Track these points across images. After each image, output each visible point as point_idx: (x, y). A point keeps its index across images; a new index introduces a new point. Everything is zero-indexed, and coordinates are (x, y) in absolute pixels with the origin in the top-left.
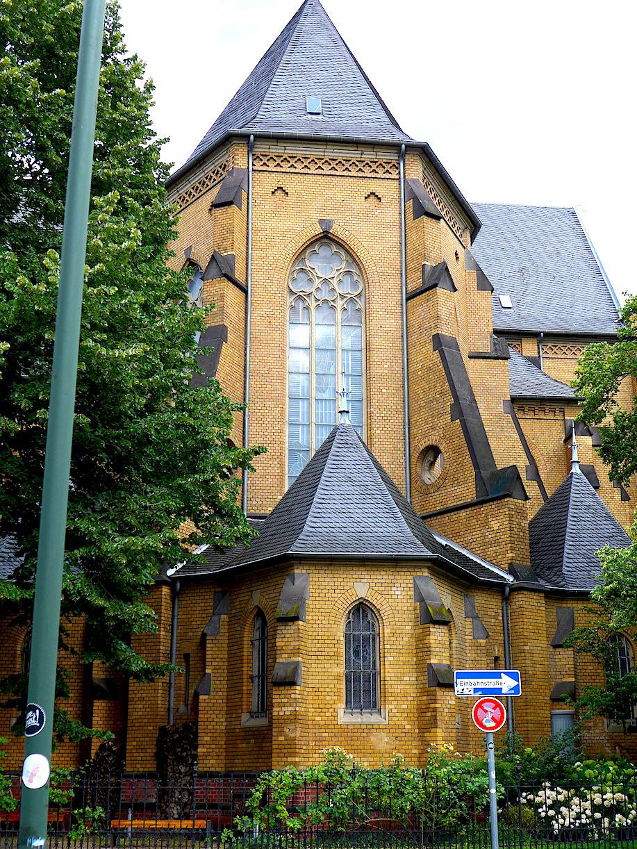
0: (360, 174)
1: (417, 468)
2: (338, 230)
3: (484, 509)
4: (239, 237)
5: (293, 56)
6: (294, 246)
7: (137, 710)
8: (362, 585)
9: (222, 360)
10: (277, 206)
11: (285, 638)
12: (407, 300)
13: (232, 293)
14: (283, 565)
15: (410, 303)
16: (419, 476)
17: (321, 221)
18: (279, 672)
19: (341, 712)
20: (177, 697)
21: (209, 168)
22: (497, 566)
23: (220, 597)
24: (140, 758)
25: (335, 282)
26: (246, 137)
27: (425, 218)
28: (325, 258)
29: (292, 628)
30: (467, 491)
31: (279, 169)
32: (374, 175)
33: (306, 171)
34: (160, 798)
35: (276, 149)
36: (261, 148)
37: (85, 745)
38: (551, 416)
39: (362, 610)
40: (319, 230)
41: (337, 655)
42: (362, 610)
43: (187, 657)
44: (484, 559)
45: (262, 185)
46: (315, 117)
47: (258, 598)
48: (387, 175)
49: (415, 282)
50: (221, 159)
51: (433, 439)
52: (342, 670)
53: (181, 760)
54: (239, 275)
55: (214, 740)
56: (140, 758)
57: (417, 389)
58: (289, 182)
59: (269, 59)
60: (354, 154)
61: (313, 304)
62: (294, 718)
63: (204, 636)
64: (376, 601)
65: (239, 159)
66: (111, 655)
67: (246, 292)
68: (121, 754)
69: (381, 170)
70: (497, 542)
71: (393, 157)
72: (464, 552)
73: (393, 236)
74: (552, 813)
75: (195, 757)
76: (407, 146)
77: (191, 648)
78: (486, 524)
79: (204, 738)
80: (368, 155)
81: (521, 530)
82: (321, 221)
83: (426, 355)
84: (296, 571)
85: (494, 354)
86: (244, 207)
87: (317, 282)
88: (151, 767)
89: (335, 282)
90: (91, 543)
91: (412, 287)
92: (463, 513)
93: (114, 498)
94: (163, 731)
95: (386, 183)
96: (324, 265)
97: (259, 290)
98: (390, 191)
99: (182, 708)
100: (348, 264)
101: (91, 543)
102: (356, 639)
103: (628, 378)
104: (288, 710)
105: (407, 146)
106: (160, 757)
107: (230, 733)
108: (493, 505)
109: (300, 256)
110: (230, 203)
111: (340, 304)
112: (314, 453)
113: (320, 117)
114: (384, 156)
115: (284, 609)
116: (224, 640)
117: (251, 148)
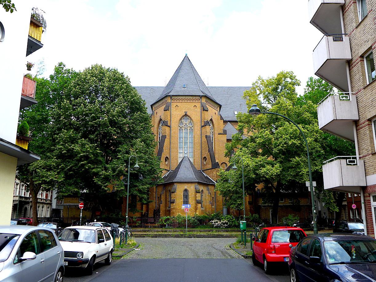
1: (203, 161)
2: (188, 114)
4: (169, 116)
5: (182, 73)
6: (179, 118)
7: (150, 207)
8: (186, 186)
9: (165, 142)
10: (176, 109)
11: (173, 195)
13: (167, 128)
14: (173, 183)
16: (203, 162)
17: (185, 112)
18: (172, 201)
20: (157, 204)
21: (164, 100)
23: (164, 187)
24: (151, 215)
25: (188, 124)
27: (205, 111)
28: (186, 119)
29: (174, 194)
30: (210, 166)
34: (154, 221)
35: (176, 97)
36: (173, 98)
37: (142, 213)
39: (186, 190)
40: (184, 114)
41: (182, 198)
42: (186, 190)
43: (159, 197)
44: (212, 179)
45: (173, 105)
47: (169, 188)
48: (198, 102)
49: (203, 124)
50: (166, 99)
52: (183, 200)
53: (157, 215)
54: (169, 124)
55: (163, 212)
56: (151, 215)
57: (203, 146)
58: (178, 104)
59: (177, 72)
60: (191, 98)
61: (183, 128)
62: (174, 208)
63: (161, 194)
64: (188, 189)
65: (169, 100)
66: (141, 201)
68: (148, 214)
69: (197, 101)
71: (199, 98)
72: (209, 178)
73: (199, 114)
74: (214, 224)
75: (160, 214)
77: (159, 196)
79: (161, 211)
80: (194, 98)
82: (185, 112)
83: (204, 139)
84: (175, 184)
85: (223, 134)
86: (170, 110)
87: (184, 124)
88: (153, 216)
89: (188, 124)
90: (138, 187)
92: (210, 170)
94: (154, 210)
95: (197, 103)
96: (186, 122)
97: (173, 127)
98: (199, 105)
99: (158, 206)
100: (190, 120)
101: (138, 187)
102: (185, 195)
103: (334, 87)
104: (173, 207)
106: (154, 214)
107: (165, 210)
108: (214, 169)
109: (181, 119)
110: (167, 110)
111: (189, 128)
113: (185, 89)
114: (197, 98)
115: (172, 191)
116: (164, 195)
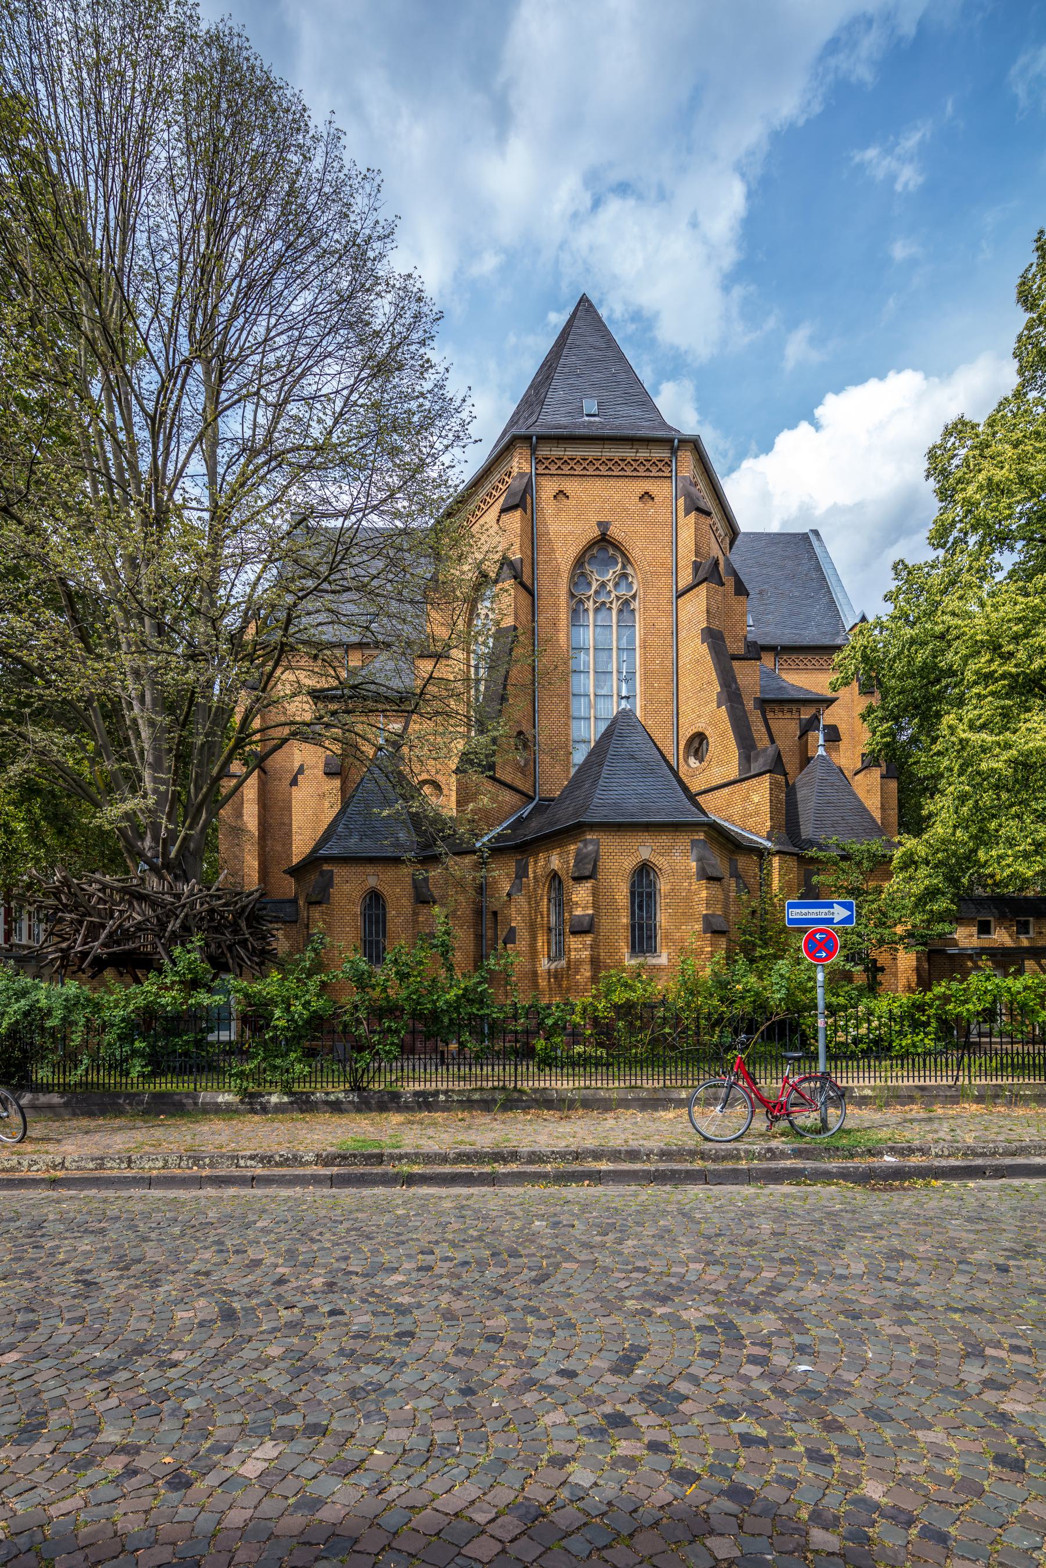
0: (635, 474)
3: (745, 785)
10: (560, 510)
12: (678, 597)
15: (680, 601)
17: (600, 524)
19: (627, 956)
22: (757, 834)
26: (527, 438)
31: (559, 472)
32: (647, 474)
33: (585, 472)
36: (543, 452)
38: (788, 716)
40: (596, 532)
46: (592, 419)
51: (700, 726)
54: (526, 579)
58: (571, 486)
60: (629, 453)
64: (385, 890)
67: (533, 596)
69: (654, 469)
70: (757, 814)
71: (665, 454)
76: (680, 441)
78: (747, 798)
81: (780, 802)
82: (600, 524)
91: (682, 584)
93: (98, 567)
95: (659, 482)
105: (680, 441)
112: (593, 744)
113: (597, 419)
117: (533, 450)
